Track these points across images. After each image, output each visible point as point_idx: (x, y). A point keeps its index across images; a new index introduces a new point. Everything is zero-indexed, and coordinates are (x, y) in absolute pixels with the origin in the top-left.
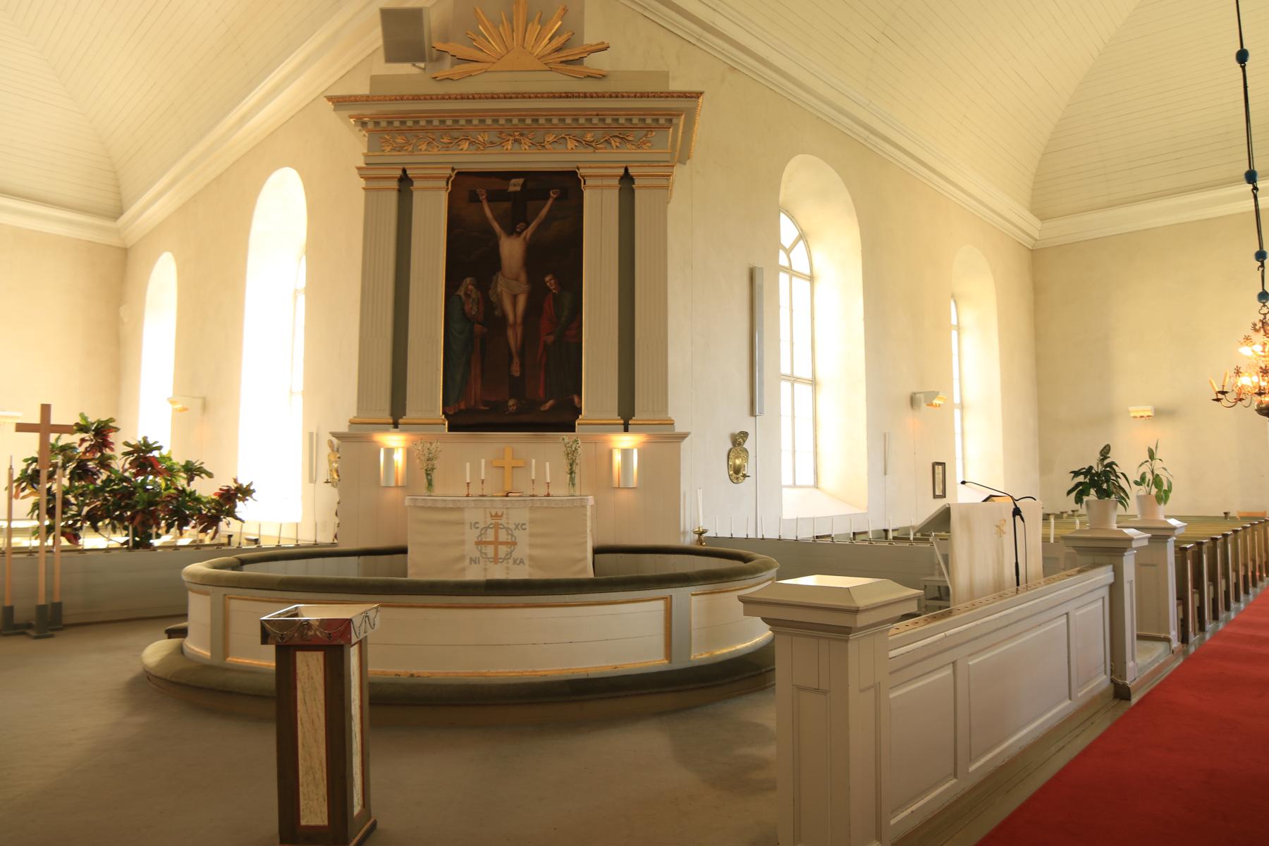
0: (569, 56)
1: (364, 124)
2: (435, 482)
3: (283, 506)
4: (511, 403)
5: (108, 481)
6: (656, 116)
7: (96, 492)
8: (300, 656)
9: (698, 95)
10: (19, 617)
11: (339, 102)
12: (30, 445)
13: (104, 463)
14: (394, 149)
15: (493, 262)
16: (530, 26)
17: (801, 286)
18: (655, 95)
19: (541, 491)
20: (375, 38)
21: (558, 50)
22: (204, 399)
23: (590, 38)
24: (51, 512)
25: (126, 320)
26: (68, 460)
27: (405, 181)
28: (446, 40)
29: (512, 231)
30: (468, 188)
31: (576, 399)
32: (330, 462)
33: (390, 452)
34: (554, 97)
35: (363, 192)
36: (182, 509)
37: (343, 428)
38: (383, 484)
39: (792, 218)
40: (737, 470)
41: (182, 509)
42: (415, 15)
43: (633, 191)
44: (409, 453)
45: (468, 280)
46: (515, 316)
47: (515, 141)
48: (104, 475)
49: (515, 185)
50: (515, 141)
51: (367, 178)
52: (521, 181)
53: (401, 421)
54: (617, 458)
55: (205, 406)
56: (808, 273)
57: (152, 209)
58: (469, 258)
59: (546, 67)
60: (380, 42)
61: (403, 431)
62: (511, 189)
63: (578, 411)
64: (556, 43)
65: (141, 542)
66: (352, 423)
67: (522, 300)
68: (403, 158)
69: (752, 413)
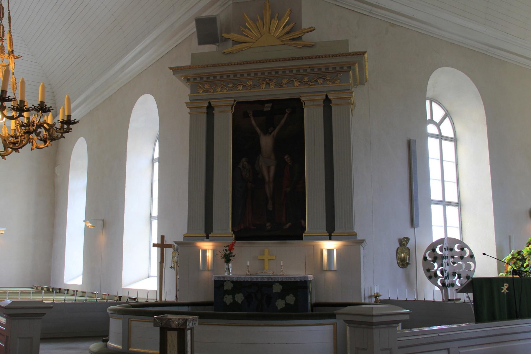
0: (294, 33)
1: (188, 80)
4: (268, 224)
8: (169, 333)
9: (364, 53)
11: (176, 70)
14: (204, 92)
15: (257, 149)
16: (273, 21)
17: (448, 146)
18: (340, 55)
20: (193, 28)
21: (288, 33)
22: (103, 221)
23: (305, 25)
25: (58, 175)
27: (210, 109)
28: (228, 31)
29: (266, 132)
30: (243, 110)
31: (303, 222)
32: (173, 257)
33: (204, 252)
34: (286, 60)
35: (189, 115)
37: (181, 239)
38: (201, 268)
39: (440, 104)
42: (212, 20)
43: (331, 107)
44: (214, 252)
45: (244, 159)
46: (269, 178)
47: (267, 83)
49: (267, 107)
50: (267, 83)
52: (270, 105)
53: (210, 235)
54: (325, 253)
55: (104, 224)
56: (452, 136)
58: (244, 147)
59: (281, 43)
60: (195, 30)
61: (211, 241)
62: (266, 109)
63: (305, 229)
64: (286, 30)
66: (185, 237)
67: (272, 169)
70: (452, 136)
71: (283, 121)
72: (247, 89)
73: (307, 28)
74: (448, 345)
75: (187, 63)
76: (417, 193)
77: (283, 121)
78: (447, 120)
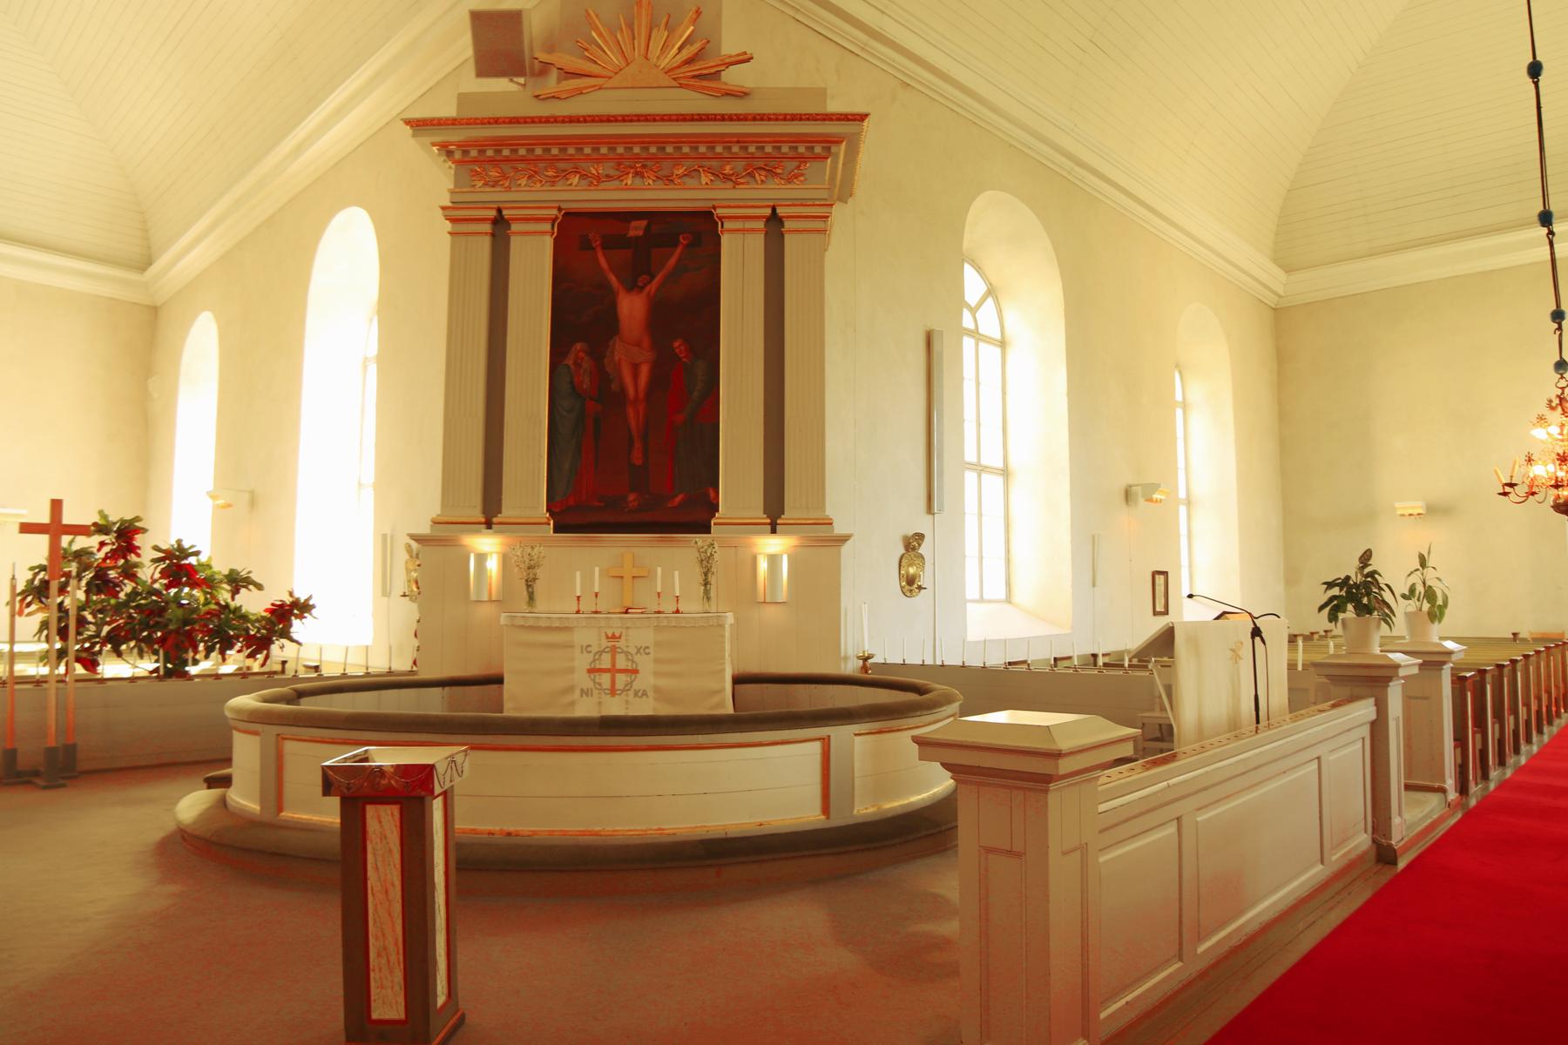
0: (701, 69)
1: (449, 154)
2: (537, 596)
3: (350, 625)
4: (631, 497)
5: (134, 594)
6: (808, 144)
7: (119, 609)
9: (862, 117)
10: (22, 762)
11: (419, 125)
12: (38, 549)
13: (129, 573)
14: (486, 184)
15: (609, 323)
17: (990, 353)
19: (669, 607)
20: (464, 47)
21: (689, 61)
22: (252, 493)
23: (730, 46)
24: (63, 633)
26: (84, 568)
28: (551, 49)
29: (633, 287)
30: (575, 233)
31: (712, 494)
33: (481, 558)
36: (224, 629)
37: (425, 529)
38: (473, 597)
39: (979, 269)
40: (911, 581)
41: (224, 629)
42: (513, 19)
43: (782, 235)
44: (505, 560)
45: (578, 346)
48: (128, 587)
49: (637, 229)
51: (453, 220)
52: (645, 223)
54: (763, 566)
55: (253, 502)
56: (998, 337)
57: (187, 258)
58: (578, 321)
60: (469, 52)
62: (631, 233)
63: (715, 508)
64: (686, 54)
65: (175, 671)
67: (645, 371)
68: (497, 196)
69: (930, 509)
70: (998, 337)
71: (672, 261)
72: (591, 184)
73: (734, 53)
74: (1173, 811)
75: (447, 109)
76: (941, 442)
77: (672, 261)
78: (990, 300)
